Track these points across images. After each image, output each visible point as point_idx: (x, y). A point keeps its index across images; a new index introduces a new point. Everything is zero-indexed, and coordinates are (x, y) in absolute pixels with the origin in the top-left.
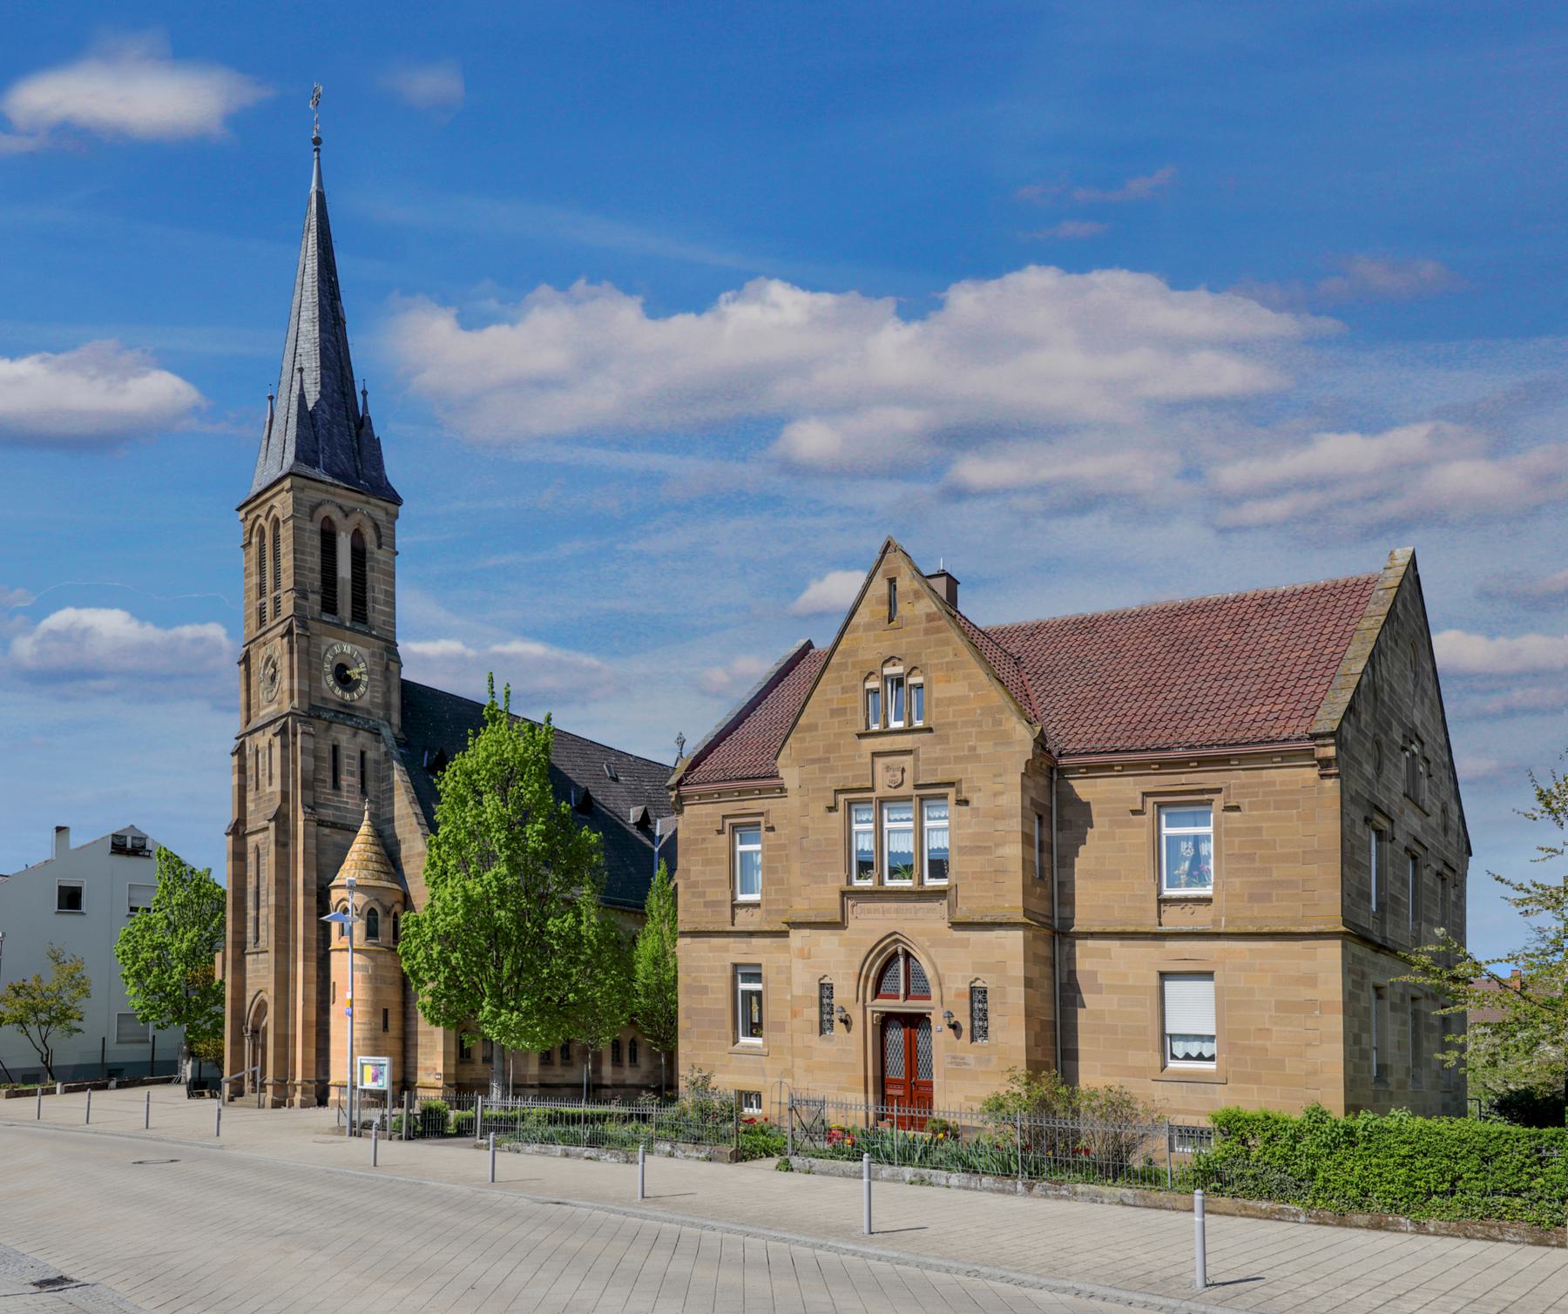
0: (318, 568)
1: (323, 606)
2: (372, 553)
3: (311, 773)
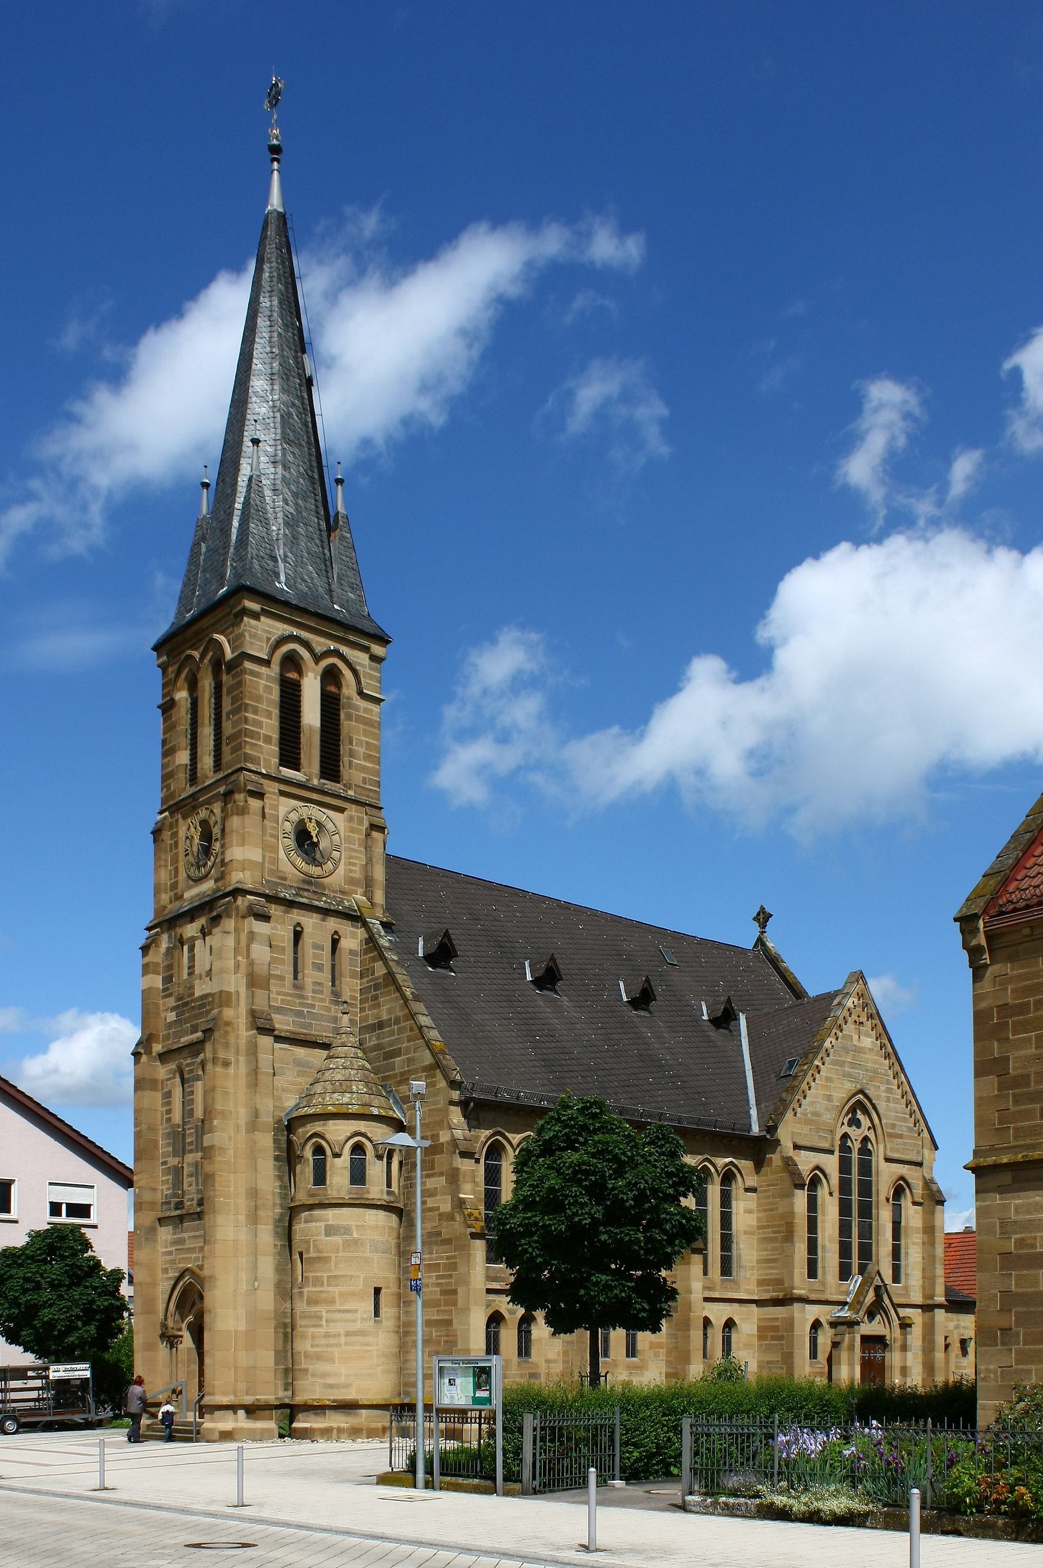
0: (276, 736)
1: (281, 760)
2: (350, 706)
3: (266, 967)
